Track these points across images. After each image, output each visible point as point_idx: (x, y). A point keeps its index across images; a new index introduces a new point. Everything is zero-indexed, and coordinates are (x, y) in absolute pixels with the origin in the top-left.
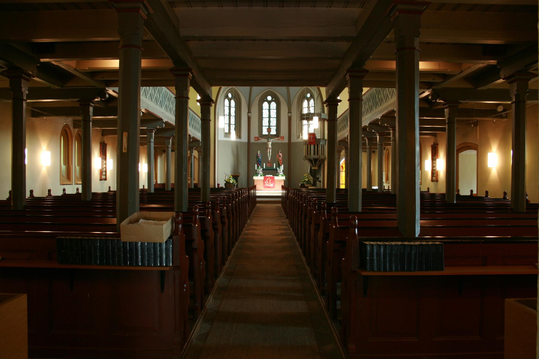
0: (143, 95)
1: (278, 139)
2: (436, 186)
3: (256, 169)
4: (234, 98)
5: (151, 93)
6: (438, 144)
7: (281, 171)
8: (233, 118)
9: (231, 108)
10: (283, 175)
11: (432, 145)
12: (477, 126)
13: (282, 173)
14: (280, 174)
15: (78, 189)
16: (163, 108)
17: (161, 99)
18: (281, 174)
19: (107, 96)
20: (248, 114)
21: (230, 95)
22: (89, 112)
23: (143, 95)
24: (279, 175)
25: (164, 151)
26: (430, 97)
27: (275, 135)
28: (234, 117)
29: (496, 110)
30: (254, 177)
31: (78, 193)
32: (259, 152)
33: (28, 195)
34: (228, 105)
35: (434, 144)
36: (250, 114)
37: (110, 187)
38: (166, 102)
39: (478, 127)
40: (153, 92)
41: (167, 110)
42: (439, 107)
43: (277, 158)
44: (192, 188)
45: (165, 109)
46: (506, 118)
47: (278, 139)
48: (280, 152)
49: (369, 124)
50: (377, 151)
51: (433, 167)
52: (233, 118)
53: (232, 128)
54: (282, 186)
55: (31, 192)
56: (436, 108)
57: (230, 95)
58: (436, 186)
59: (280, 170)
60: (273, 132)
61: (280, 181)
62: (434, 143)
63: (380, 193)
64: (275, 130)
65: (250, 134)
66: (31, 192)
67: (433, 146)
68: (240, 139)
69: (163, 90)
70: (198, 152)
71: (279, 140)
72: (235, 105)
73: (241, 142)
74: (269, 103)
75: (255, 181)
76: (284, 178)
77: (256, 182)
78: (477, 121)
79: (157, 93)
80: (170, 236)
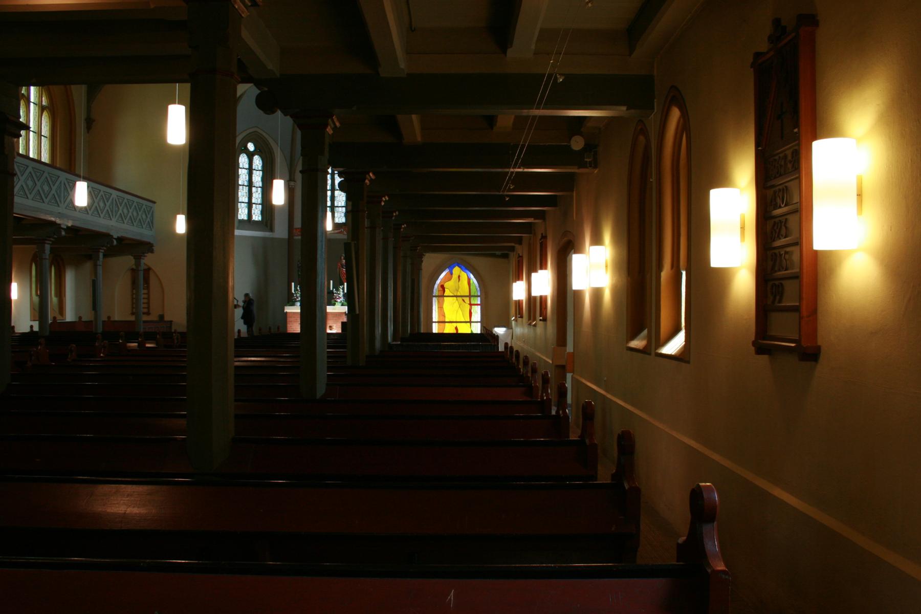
1: (339, 231)
3: (331, 289)
4: (260, 151)
7: (341, 295)
8: (257, 192)
9: (254, 172)
10: (345, 303)
12: (573, 191)
13: (342, 299)
14: (339, 300)
15: (32, 327)
18: (341, 302)
20: (289, 183)
21: (251, 147)
24: (336, 303)
25: (89, 257)
27: (343, 223)
28: (260, 190)
29: (569, 147)
30: (286, 307)
31: (32, 331)
34: (247, 166)
39: (574, 192)
43: (338, 270)
44: (178, 83)
46: (596, 167)
47: (339, 231)
48: (342, 258)
50: (777, 251)
52: (257, 192)
53: (257, 178)
57: (251, 147)
59: (339, 294)
60: (257, 216)
61: (339, 315)
64: (343, 215)
65: (293, 221)
68: (271, 233)
70: (134, 258)
71: (341, 235)
72: (263, 166)
73: (272, 239)
74: (250, 156)
75: (288, 316)
76: (345, 309)
77: (291, 317)
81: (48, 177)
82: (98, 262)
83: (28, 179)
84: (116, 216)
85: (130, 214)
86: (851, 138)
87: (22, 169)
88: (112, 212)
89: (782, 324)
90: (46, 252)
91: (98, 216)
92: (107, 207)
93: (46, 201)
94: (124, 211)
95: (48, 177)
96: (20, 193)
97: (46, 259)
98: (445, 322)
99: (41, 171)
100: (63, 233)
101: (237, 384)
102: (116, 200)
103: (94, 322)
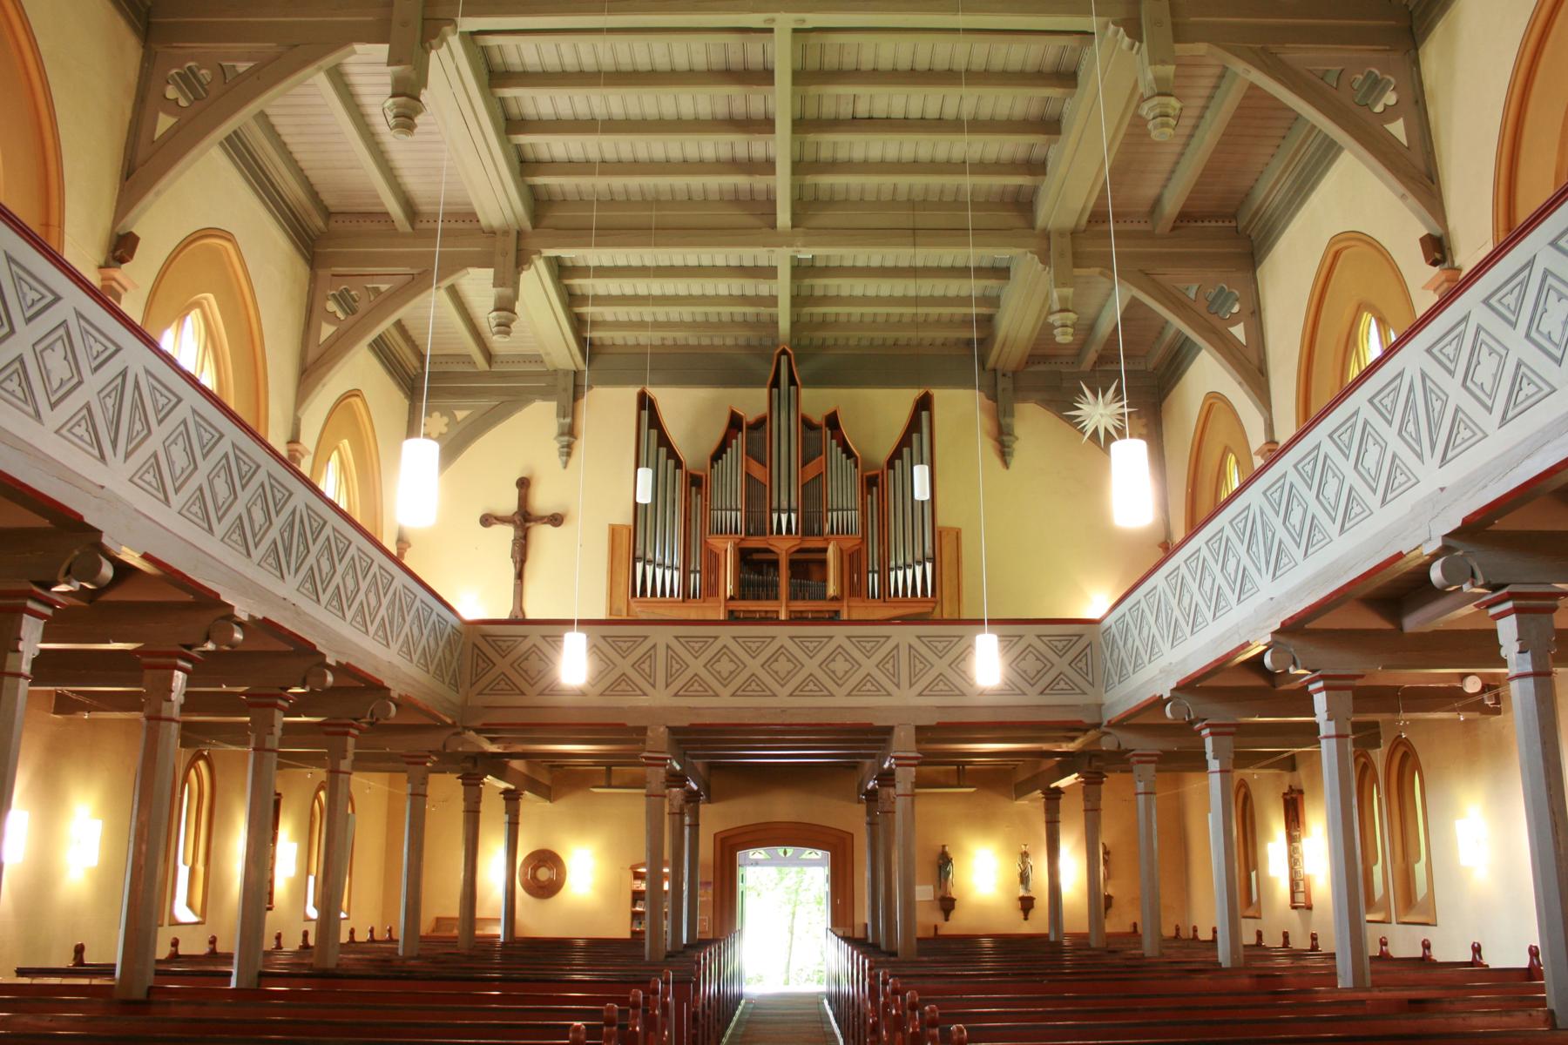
0: (332, 609)
2: (1306, 923)
5: (407, 636)
6: (1301, 792)
11: (1285, 794)
16: (395, 647)
17: (383, 612)
19: (107, 571)
22: (171, 691)
23: (332, 609)
26: (1267, 660)
32: (678, 768)
33: (344, 938)
35: (1291, 789)
37: (372, 931)
38: (407, 624)
40: (373, 602)
41: (427, 666)
42: (1297, 685)
45: (400, 650)
49: (1173, 690)
51: (1293, 861)
54: (426, 88)
55: (352, 932)
56: (1285, 687)
58: (1306, 923)
62: (1290, 787)
63: (1150, 958)
66: (352, 932)
67: (1288, 797)
69: (395, 580)
78: (1293, 757)
79: (429, 635)
80: (1459, 529)
81: (378, 574)
82: (165, 705)
83: (175, 442)
84: (297, 570)
85: (199, 479)
86: (1078, 64)
87: (162, 401)
88: (391, 623)
89: (1300, 898)
90: (174, 696)
91: (364, 629)
92: (274, 533)
93: (115, 461)
94: (322, 561)
95: (378, 574)
96: (77, 430)
97: (20, 675)
98: (1145, 793)
99: (216, 429)
100: (330, 678)
101: (743, 1002)
102: (302, 521)
103: (647, 936)
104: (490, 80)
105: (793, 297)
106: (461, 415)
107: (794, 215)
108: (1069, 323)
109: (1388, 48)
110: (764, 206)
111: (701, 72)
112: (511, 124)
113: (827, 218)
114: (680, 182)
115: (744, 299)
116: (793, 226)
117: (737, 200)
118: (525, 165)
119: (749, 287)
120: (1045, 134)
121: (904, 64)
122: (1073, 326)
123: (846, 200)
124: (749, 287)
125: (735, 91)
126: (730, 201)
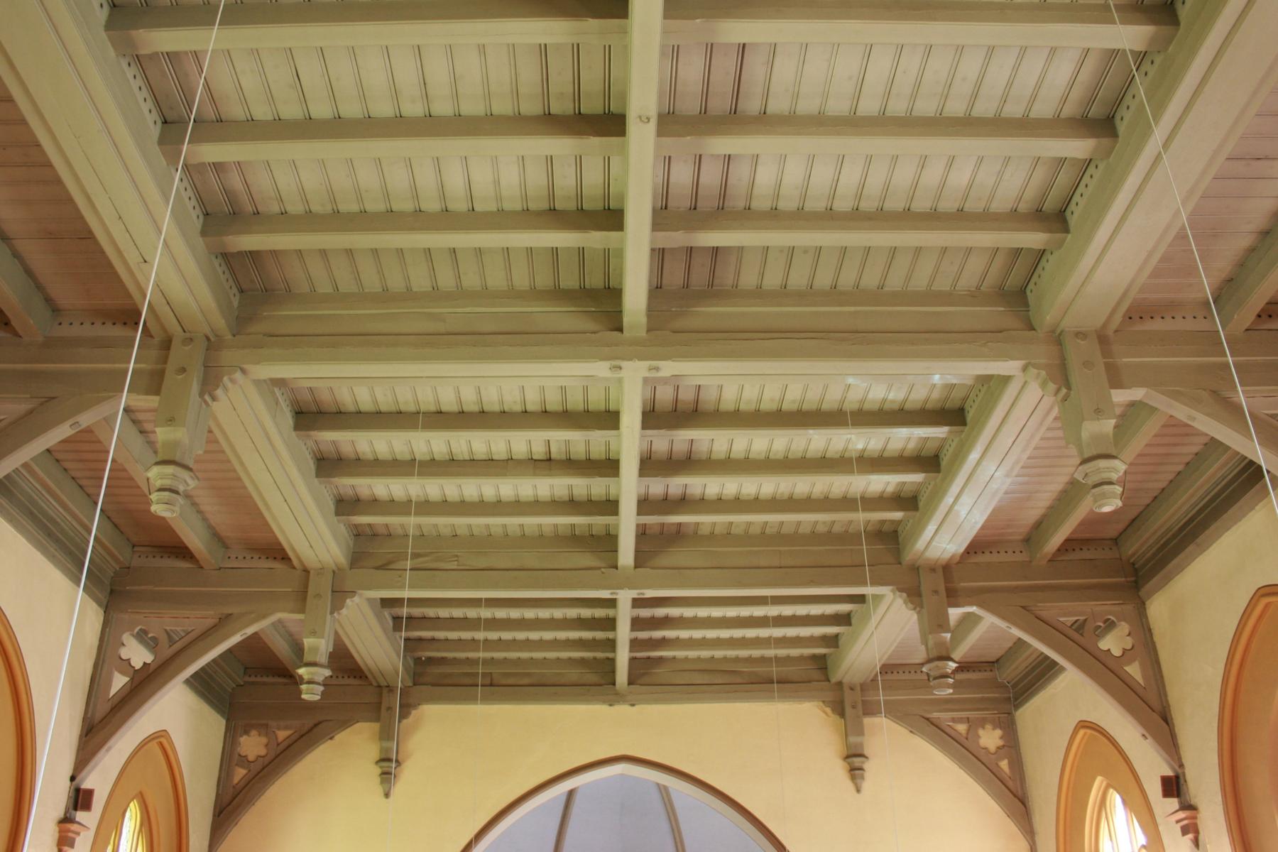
36: (852, 739)
50: (70, 835)
104: (205, 225)
105: (655, 212)
106: (282, 735)
107: (638, 552)
108: (1114, 476)
109: (996, 712)
110: (607, 543)
111: (545, 503)
112: (328, 464)
113: (678, 556)
114: (513, 522)
115: (572, 505)
116: (636, 567)
117: (576, 540)
118: (346, 505)
119: (580, 486)
120: (923, 473)
121: (768, 405)
122: (1122, 482)
123: (702, 500)
124: (580, 486)
125: (561, 146)
126: (539, 214)
